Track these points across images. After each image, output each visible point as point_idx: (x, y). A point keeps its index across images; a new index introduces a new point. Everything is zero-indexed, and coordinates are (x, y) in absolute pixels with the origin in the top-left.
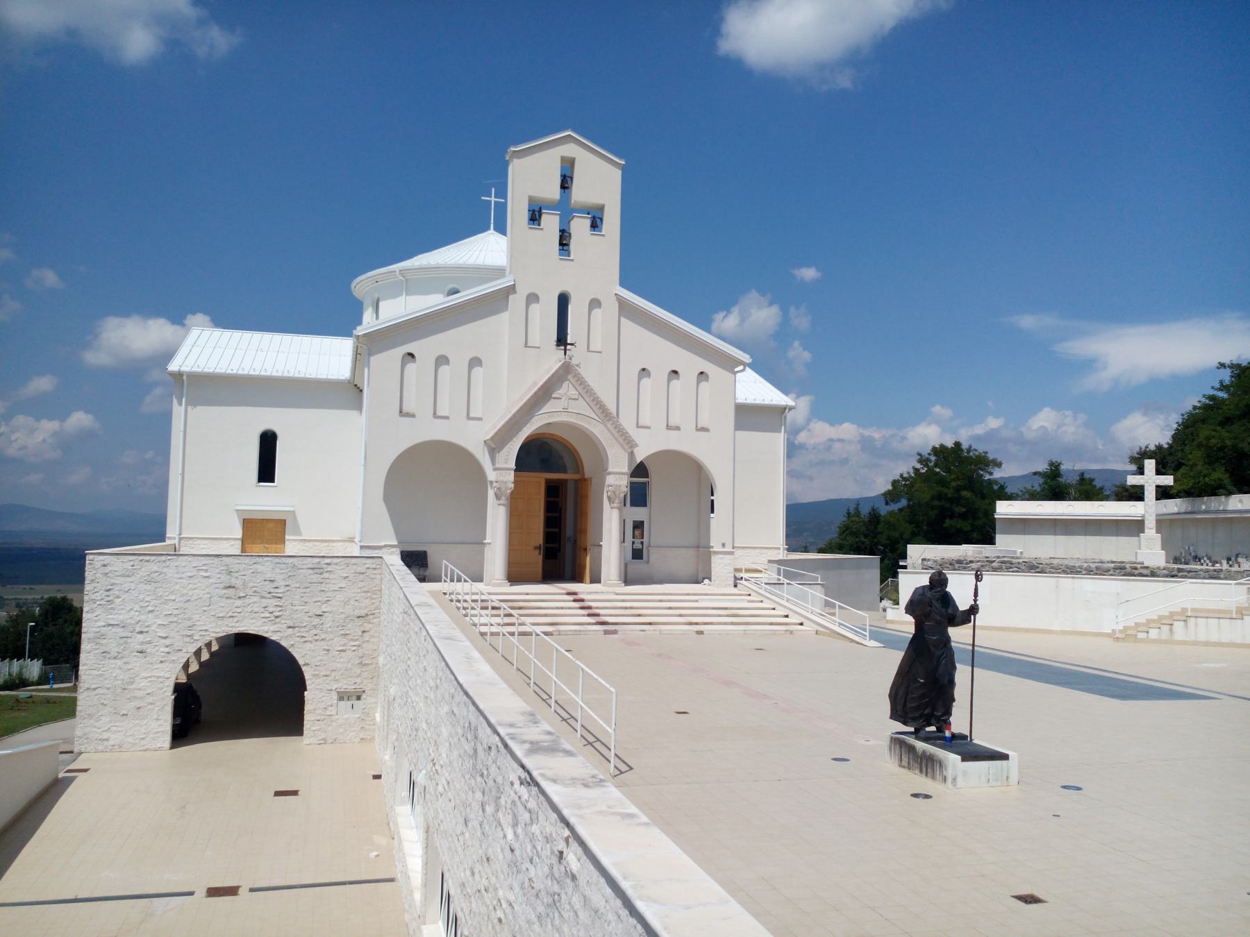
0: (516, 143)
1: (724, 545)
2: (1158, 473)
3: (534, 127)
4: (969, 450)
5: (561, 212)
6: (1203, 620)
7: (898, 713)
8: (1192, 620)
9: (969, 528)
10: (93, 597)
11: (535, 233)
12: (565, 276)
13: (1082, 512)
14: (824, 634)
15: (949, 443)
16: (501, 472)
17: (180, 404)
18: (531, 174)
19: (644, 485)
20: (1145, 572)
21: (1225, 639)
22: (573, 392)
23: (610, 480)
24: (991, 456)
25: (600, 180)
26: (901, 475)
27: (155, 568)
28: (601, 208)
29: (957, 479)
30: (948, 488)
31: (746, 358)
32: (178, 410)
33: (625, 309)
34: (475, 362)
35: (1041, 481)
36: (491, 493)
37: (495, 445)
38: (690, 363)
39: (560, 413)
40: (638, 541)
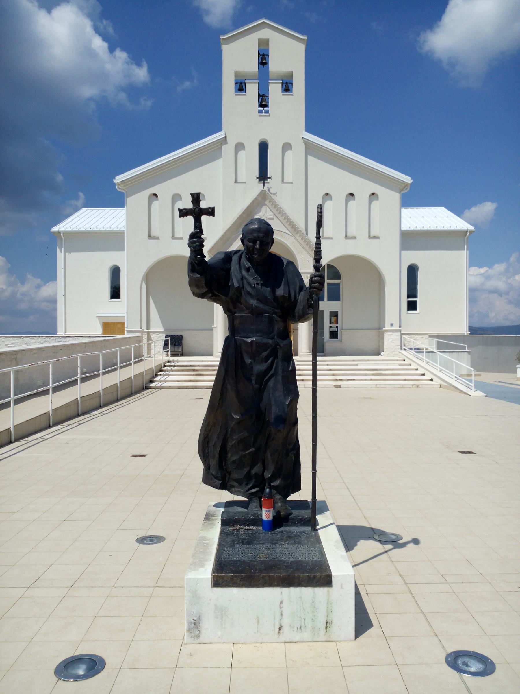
1: (392, 325)
7: (217, 475)
11: (241, 98)
12: (266, 128)
14: (445, 387)
17: (61, 252)
19: (339, 284)
25: (289, 53)
28: (290, 75)
32: (60, 255)
33: (310, 149)
38: (363, 187)
40: (333, 326)
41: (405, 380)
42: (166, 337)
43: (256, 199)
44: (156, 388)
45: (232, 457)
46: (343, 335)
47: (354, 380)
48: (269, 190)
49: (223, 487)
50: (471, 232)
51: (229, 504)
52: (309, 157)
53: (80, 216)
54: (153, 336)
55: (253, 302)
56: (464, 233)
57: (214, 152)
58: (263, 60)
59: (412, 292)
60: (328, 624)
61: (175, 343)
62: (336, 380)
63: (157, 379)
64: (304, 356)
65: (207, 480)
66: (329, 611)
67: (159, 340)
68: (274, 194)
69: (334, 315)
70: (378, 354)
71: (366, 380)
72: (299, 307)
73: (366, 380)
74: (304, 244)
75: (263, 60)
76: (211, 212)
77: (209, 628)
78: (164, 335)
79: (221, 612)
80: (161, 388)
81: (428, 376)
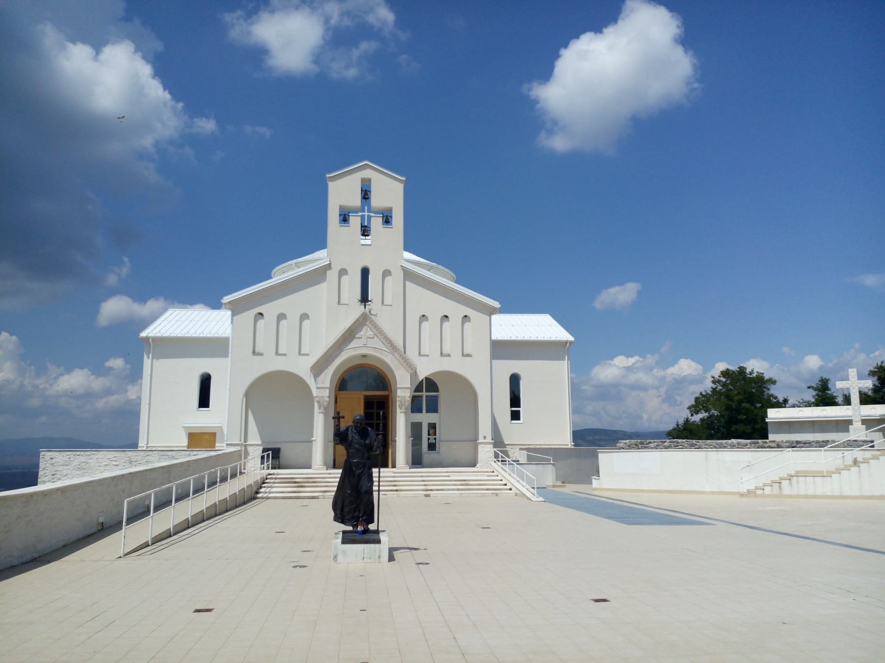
0: (330, 172)
1: (485, 438)
2: (846, 379)
3: (344, 158)
4: (751, 373)
5: (365, 215)
6: (803, 478)
8: (795, 478)
9: (750, 431)
10: (44, 479)
11: (344, 229)
13: (833, 414)
15: (734, 368)
16: (322, 388)
18: (342, 191)
19: (437, 397)
20: (773, 445)
21: (819, 492)
22: (370, 333)
23: (399, 393)
24: (767, 376)
25: (389, 191)
26: (701, 394)
27: (83, 460)
29: (739, 394)
30: (732, 400)
31: (496, 305)
32: (147, 362)
34: (304, 317)
35: (814, 393)
36: (316, 405)
37: (317, 369)
38: (457, 310)
39: (363, 347)
41: (488, 489)
42: (265, 450)
43: (357, 320)
44: (263, 498)
45: (346, 510)
46: (441, 447)
47: (443, 490)
48: (370, 312)
49: (342, 522)
50: (571, 343)
51: (344, 532)
52: (408, 283)
53: (169, 319)
54: (250, 449)
55: (357, 446)
56: (564, 343)
57: (318, 276)
58: (366, 195)
59: (515, 401)
60: (379, 557)
61: (273, 456)
62: (427, 490)
63: (262, 490)
64: (401, 468)
65: (336, 519)
66: (380, 552)
67: (256, 453)
68: (375, 315)
69: (432, 427)
70: (474, 466)
71: (453, 490)
72: (375, 447)
73: (453, 490)
74: (402, 361)
75: (366, 195)
76: (343, 417)
77: (340, 558)
78: (261, 448)
79: (344, 552)
80: (268, 498)
81: (508, 487)
